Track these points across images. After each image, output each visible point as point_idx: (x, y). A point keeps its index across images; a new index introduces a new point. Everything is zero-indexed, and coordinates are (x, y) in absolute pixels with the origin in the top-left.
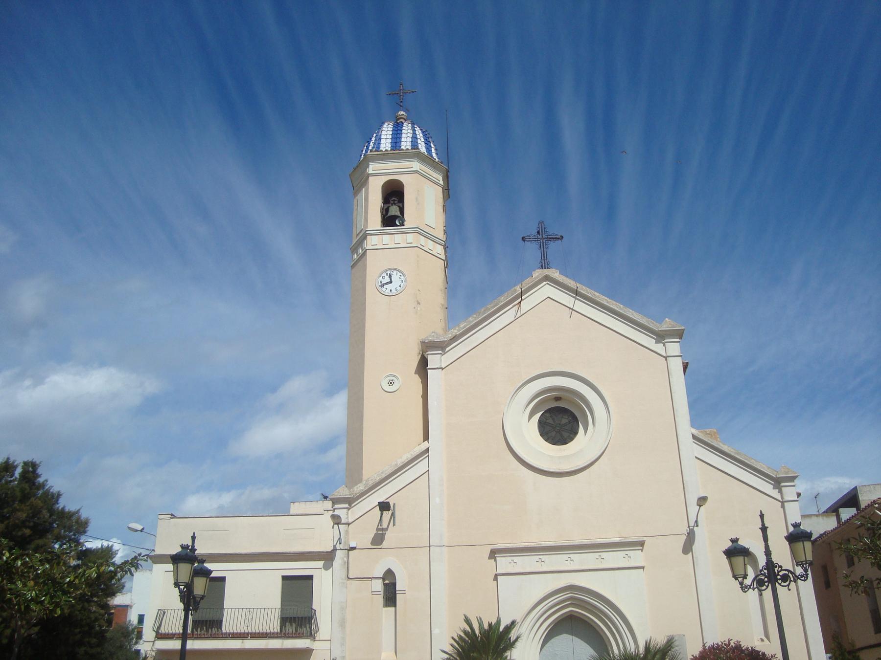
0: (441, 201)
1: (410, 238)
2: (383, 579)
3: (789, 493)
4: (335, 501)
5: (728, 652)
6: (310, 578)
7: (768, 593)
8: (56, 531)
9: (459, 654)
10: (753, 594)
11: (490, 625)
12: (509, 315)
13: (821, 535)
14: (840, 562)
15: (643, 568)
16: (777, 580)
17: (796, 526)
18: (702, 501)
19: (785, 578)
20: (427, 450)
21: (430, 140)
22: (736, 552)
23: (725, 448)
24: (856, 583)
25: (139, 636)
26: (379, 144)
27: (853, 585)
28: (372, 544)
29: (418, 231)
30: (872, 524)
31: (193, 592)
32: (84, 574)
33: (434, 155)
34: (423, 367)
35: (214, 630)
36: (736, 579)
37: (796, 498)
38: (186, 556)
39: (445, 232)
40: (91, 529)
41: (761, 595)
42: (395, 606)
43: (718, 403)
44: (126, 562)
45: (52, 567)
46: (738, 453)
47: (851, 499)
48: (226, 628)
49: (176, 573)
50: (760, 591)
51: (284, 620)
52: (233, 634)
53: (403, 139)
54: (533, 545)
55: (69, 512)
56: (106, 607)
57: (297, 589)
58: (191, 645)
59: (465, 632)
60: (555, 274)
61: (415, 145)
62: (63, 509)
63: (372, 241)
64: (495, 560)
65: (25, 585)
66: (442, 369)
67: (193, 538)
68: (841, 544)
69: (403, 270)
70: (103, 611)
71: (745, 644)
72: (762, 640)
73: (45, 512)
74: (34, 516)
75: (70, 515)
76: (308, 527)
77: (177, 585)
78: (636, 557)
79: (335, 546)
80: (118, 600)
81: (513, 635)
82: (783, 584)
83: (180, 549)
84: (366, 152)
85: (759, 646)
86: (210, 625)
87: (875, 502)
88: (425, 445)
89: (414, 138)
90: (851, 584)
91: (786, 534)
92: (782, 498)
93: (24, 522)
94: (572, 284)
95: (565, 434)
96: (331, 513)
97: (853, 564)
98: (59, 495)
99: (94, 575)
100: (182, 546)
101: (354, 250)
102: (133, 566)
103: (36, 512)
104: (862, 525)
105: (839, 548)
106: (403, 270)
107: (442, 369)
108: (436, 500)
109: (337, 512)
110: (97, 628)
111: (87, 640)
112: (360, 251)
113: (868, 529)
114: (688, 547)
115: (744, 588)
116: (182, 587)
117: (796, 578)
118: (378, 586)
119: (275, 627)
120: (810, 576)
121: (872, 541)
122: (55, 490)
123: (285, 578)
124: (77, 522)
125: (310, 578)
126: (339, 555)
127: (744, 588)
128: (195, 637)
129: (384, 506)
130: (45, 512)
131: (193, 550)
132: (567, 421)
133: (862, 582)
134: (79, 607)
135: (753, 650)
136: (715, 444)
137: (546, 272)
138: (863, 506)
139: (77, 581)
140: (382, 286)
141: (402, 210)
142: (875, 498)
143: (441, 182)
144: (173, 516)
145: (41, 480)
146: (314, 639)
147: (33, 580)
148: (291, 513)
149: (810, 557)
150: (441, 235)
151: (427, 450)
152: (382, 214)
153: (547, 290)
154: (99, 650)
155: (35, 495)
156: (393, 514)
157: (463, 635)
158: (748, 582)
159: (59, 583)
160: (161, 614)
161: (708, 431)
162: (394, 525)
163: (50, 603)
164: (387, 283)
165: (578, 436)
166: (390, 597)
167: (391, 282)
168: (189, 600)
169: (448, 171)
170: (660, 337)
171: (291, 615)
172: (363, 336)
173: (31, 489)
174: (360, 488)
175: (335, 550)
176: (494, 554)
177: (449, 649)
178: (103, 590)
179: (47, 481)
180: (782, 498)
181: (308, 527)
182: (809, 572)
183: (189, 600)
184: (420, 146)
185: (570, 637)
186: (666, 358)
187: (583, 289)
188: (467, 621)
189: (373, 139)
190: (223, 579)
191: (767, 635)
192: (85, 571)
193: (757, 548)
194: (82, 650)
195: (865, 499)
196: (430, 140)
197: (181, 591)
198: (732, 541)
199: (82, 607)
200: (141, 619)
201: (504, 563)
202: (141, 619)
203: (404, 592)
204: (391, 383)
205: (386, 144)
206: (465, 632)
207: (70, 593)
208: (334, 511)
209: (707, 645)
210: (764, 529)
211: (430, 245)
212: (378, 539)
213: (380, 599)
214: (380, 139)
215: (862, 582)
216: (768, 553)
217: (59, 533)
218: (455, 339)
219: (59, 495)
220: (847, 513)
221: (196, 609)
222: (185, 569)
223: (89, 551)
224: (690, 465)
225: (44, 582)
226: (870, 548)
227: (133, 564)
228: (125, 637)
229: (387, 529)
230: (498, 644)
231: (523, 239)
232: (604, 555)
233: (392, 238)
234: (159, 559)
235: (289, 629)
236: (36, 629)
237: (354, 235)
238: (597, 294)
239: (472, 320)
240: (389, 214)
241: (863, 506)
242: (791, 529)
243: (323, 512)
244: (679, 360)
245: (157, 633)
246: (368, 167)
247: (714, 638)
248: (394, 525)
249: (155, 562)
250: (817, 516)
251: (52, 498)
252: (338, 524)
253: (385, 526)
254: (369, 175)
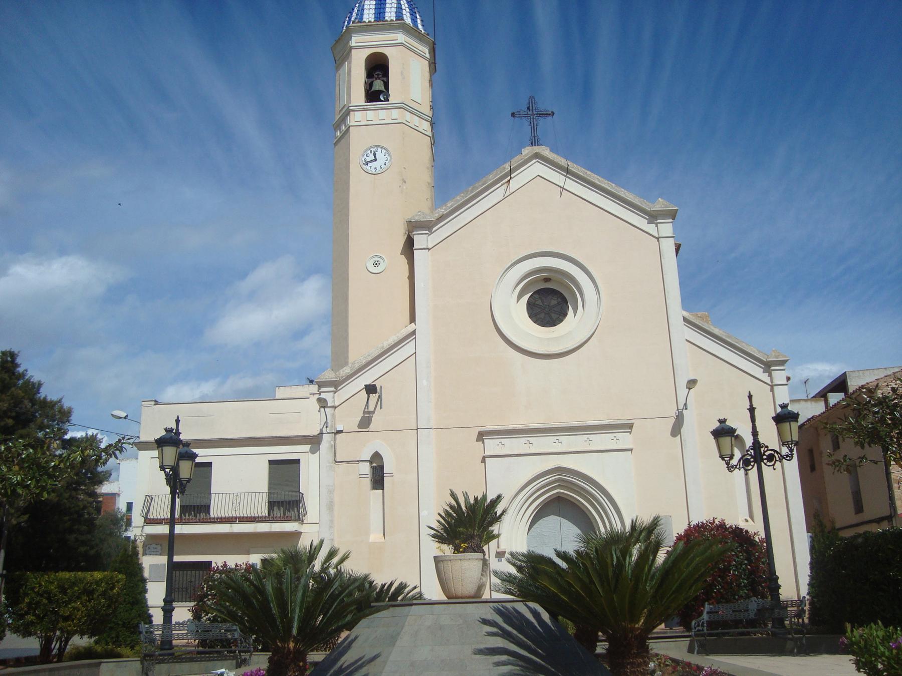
0: (427, 75)
1: (395, 113)
2: (371, 462)
3: (779, 376)
4: (321, 385)
5: (712, 529)
6: (297, 462)
8: (39, 421)
9: (445, 529)
10: (739, 474)
11: (476, 499)
12: (497, 194)
13: (809, 420)
14: (826, 446)
15: (631, 450)
16: (762, 460)
17: (784, 406)
18: (691, 384)
19: (771, 458)
20: (414, 333)
21: (416, 10)
22: (723, 432)
23: (716, 331)
24: (839, 461)
25: (129, 523)
26: (362, 14)
27: (836, 464)
28: (359, 427)
29: (403, 107)
30: (858, 404)
31: (179, 475)
32: (68, 459)
33: (420, 27)
34: (409, 247)
35: (203, 515)
36: (723, 459)
37: (785, 382)
38: (170, 439)
39: (432, 108)
40: (74, 418)
41: (746, 474)
42: (383, 489)
43: (712, 288)
44: (110, 445)
45: (35, 453)
46: (729, 337)
47: (840, 384)
48: (214, 513)
49: (161, 457)
50: (746, 470)
51: (272, 504)
52: (221, 518)
53: (387, 10)
54: (521, 427)
55: (51, 402)
56: (94, 495)
57: (284, 474)
58: (179, 529)
59: (451, 507)
60: (545, 151)
61: (399, 16)
62: (45, 398)
63: (355, 118)
64: (483, 443)
65: (10, 469)
66: (429, 249)
67: (178, 421)
68: (826, 424)
69: (388, 146)
70: (91, 499)
71: (729, 522)
72: (747, 521)
73: (26, 402)
74: (16, 406)
75: (52, 404)
76: (295, 411)
77: (162, 468)
78: (624, 439)
79: (321, 430)
80: (106, 488)
81: (499, 510)
82: (769, 464)
83: (165, 433)
84: (349, 23)
85: (742, 525)
86: (198, 510)
87: (863, 387)
88: (412, 327)
89: (399, 8)
90: (834, 463)
91: (774, 415)
92: (772, 382)
93: (5, 412)
94: (563, 161)
95: (554, 316)
96: (317, 396)
97: (839, 448)
98: (40, 384)
99: (79, 459)
100: (166, 430)
101: (337, 126)
102: (117, 449)
103: (17, 402)
104: (848, 405)
105: (825, 428)
106: (388, 146)
107: (429, 249)
108: (423, 383)
109: (323, 396)
110: (86, 516)
111: (76, 527)
112: (343, 128)
113: (854, 409)
114: (676, 430)
115: (730, 468)
116: (168, 470)
117: (782, 458)
118: (366, 469)
119: (264, 511)
120: (795, 456)
121: (856, 421)
122: (35, 379)
123: (271, 462)
124: (60, 411)
125: (297, 462)
126: (326, 438)
128: (182, 522)
129: (371, 389)
130: (26, 402)
131: (178, 433)
132: (556, 302)
133: (845, 461)
134: (67, 495)
135: (737, 528)
136: (706, 326)
137: (536, 149)
138: (851, 391)
139: (62, 465)
140: (367, 163)
141: (386, 85)
142: (863, 383)
143: (428, 56)
144: (157, 403)
145: (21, 370)
146: (302, 522)
147: (17, 464)
148: (277, 397)
149: (796, 438)
150: (426, 110)
151: (414, 333)
152: (366, 89)
153: (537, 168)
154: (89, 536)
155: (15, 385)
156: (380, 397)
157: (450, 511)
159: (44, 467)
160: (149, 500)
161: (700, 314)
162: (381, 408)
163: (36, 487)
164: (371, 161)
165: (567, 318)
166: (378, 479)
167: (375, 160)
168: (175, 483)
169: (434, 44)
170: (653, 217)
171: (279, 499)
172: (347, 215)
173: (11, 379)
174: (347, 371)
175: (321, 433)
176: (481, 436)
177: (435, 525)
178: (89, 478)
179: (26, 370)
180: (772, 382)
181: (295, 411)
182: (795, 452)
183: (175, 483)
184: (405, 17)
185: (558, 518)
186: (658, 239)
187: (574, 168)
188: (453, 495)
189: (356, 10)
190: (209, 464)
191: (751, 517)
192: (69, 455)
193: (744, 431)
194: (72, 537)
195: (853, 384)
196: (416, 10)
197: (167, 475)
198: (720, 421)
199: (70, 496)
200: (130, 506)
201: (492, 445)
202: (130, 506)
203: (391, 475)
204: (376, 264)
205: (369, 15)
206: (451, 507)
207: (55, 476)
208: (320, 394)
209: (692, 524)
210: (752, 410)
211: (416, 121)
212: (365, 422)
213: (367, 482)
214: (363, 10)
215: (845, 461)
216: (755, 433)
217: (42, 423)
218: (441, 218)
219: (40, 384)
220: (835, 398)
221: (182, 492)
222: (170, 453)
223: (73, 440)
224: (680, 347)
225: (29, 466)
226: (854, 428)
227: (116, 449)
228: (114, 525)
229: (373, 412)
230: (483, 519)
231: (513, 115)
232: (592, 437)
233: (376, 114)
234: (144, 446)
235: (277, 513)
236: (26, 517)
237: (337, 110)
238: (589, 173)
239: (460, 199)
240: (373, 89)
241: (851, 391)
242: (779, 410)
243: (308, 396)
244: (672, 241)
245: (146, 518)
246: (351, 39)
247: (700, 517)
248: (381, 408)
249: (140, 449)
250: (806, 400)
251: (33, 388)
252: (324, 407)
253: (371, 409)
254: (351, 48)
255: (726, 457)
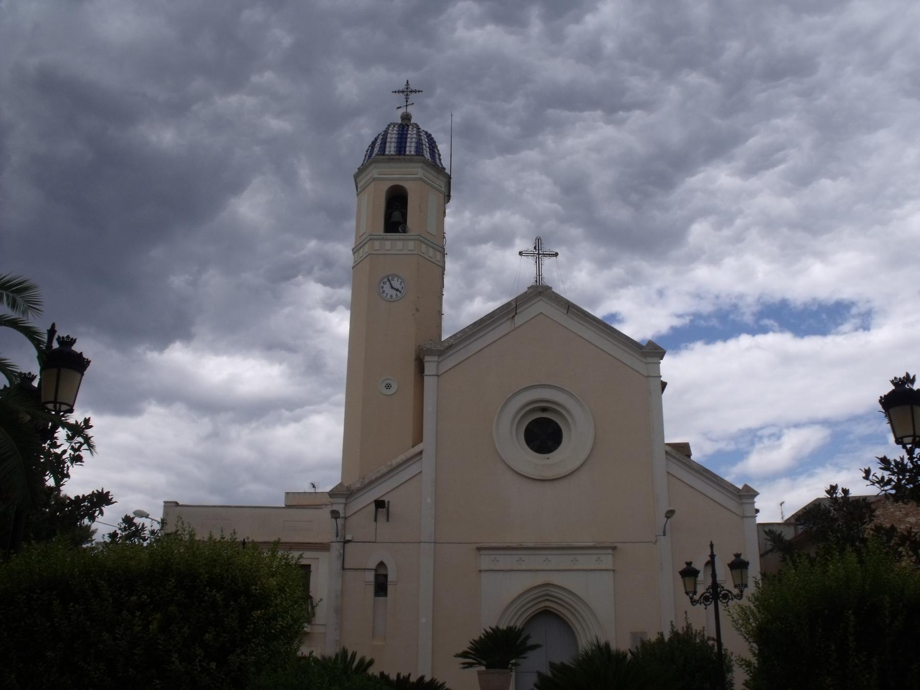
1: (411, 245)
2: (376, 570)
7: (711, 607)
19: (725, 596)
20: (421, 452)
22: (689, 573)
26: (385, 148)
115: (693, 602)
118: (371, 577)
127: (693, 602)
129: (380, 504)
143: (443, 189)
158: (696, 597)
166: (381, 587)
204: (388, 386)
209: (55, 371)
213: (371, 589)
231: (521, 253)
255: (691, 592)
